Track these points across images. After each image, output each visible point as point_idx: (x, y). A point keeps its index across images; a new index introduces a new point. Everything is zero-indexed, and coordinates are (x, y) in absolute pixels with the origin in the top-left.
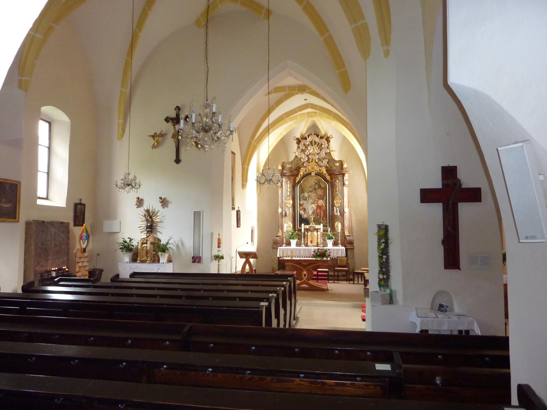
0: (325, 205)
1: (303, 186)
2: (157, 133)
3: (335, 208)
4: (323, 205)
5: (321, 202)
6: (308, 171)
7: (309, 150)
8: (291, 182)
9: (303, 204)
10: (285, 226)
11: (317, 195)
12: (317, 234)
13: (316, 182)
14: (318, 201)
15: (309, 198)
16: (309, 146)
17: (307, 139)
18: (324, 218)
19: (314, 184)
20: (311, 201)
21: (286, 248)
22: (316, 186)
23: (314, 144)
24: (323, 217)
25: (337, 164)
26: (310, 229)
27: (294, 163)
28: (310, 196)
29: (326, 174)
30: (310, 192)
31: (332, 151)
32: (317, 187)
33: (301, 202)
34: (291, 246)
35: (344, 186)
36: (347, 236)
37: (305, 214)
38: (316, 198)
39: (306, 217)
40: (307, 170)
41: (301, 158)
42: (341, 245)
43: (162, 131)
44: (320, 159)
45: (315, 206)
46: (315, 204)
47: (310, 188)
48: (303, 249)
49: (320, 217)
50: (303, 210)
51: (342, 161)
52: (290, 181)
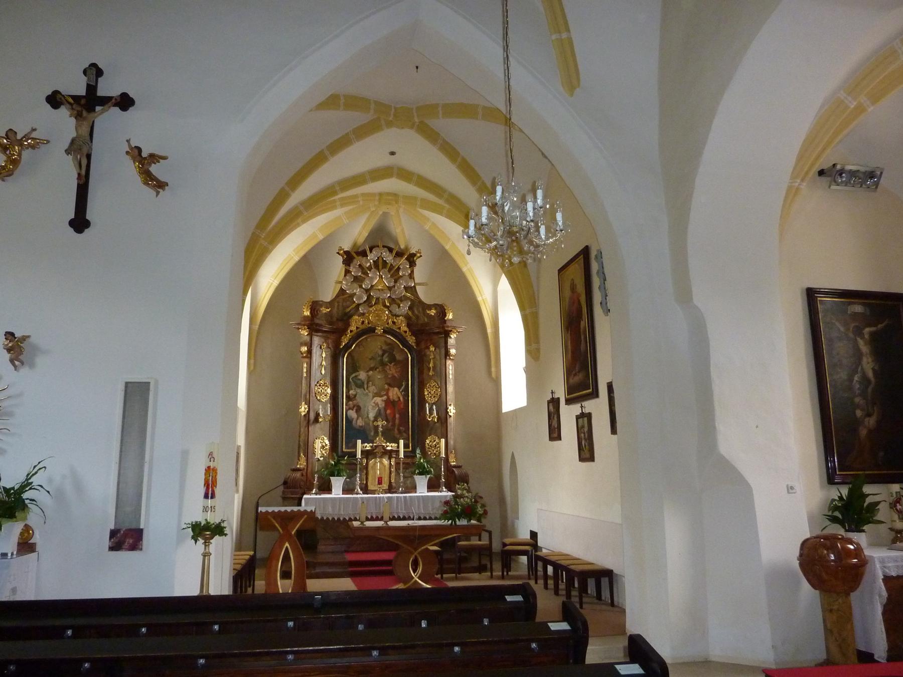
0: (404, 398)
2: (16, 133)
3: (427, 405)
4: (400, 400)
5: (395, 393)
6: (368, 323)
7: (372, 279)
8: (330, 346)
9: (355, 396)
10: (318, 444)
11: (386, 377)
12: (390, 464)
15: (368, 383)
17: (367, 256)
18: (401, 428)
19: (380, 353)
20: (372, 389)
21: (318, 496)
24: (400, 425)
25: (433, 312)
26: (375, 451)
29: (408, 331)
30: (372, 369)
31: (420, 284)
32: (386, 360)
33: (351, 392)
35: (448, 358)
36: (455, 467)
37: (360, 418)
39: (361, 425)
43: (34, 130)
45: (382, 400)
47: (372, 361)
49: (394, 425)
50: (355, 410)
51: (443, 307)
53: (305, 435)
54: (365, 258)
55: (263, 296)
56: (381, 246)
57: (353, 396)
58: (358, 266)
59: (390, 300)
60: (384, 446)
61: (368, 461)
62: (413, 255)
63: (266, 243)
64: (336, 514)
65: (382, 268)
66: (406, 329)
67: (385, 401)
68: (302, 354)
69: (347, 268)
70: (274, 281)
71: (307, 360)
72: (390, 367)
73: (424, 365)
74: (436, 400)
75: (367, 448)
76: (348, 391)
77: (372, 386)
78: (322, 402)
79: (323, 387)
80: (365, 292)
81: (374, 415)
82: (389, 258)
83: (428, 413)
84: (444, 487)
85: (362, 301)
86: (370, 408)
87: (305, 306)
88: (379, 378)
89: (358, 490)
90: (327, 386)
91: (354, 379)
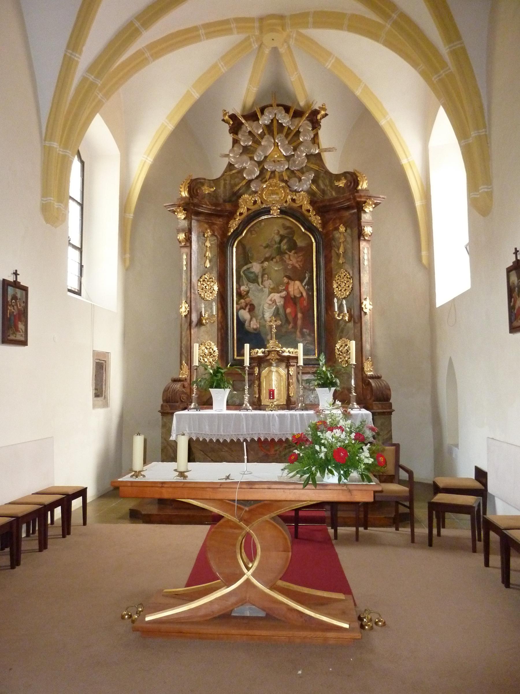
0: (308, 294)
1: (248, 247)
3: (335, 300)
5: (296, 287)
6: (262, 203)
7: (265, 148)
8: (216, 234)
9: (248, 292)
11: (285, 269)
12: (288, 373)
13: (282, 232)
14: (288, 283)
15: (262, 276)
16: (262, 138)
17: (258, 119)
18: (305, 330)
19: (277, 239)
20: (269, 283)
22: (282, 244)
23: (278, 134)
25: (341, 184)
26: (268, 358)
27: (222, 182)
28: (267, 271)
30: (267, 259)
31: (326, 150)
32: (285, 247)
33: (243, 288)
34: (212, 408)
35: (362, 238)
36: (372, 377)
37: (254, 319)
38: (283, 275)
39: (255, 327)
41: (241, 171)
42: (358, 404)
44: (293, 172)
45: (281, 297)
46: (281, 292)
47: (267, 249)
48: (305, 354)
50: (247, 310)
52: (213, 231)
53: (187, 340)
54: (256, 122)
55: (137, 178)
56: (274, 105)
57: (245, 293)
58: (248, 134)
59: (288, 173)
60: (278, 351)
61: (261, 370)
62: (315, 113)
63: (93, 77)
64: (215, 435)
65: (278, 134)
66: (309, 207)
68: (180, 242)
69: (236, 137)
70: (147, 159)
71: (186, 250)
72: (289, 256)
73: (333, 251)
74: (348, 294)
75: (259, 354)
76: (238, 289)
77: (268, 280)
78: (207, 300)
79: (209, 283)
80: (257, 165)
82: (285, 120)
83: (336, 309)
84: (355, 403)
85: (254, 177)
86: (266, 306)
87: (182, 185)
88: (276, 270)
89: (246, 405)
90: (212, 281)
91: (246, 272)
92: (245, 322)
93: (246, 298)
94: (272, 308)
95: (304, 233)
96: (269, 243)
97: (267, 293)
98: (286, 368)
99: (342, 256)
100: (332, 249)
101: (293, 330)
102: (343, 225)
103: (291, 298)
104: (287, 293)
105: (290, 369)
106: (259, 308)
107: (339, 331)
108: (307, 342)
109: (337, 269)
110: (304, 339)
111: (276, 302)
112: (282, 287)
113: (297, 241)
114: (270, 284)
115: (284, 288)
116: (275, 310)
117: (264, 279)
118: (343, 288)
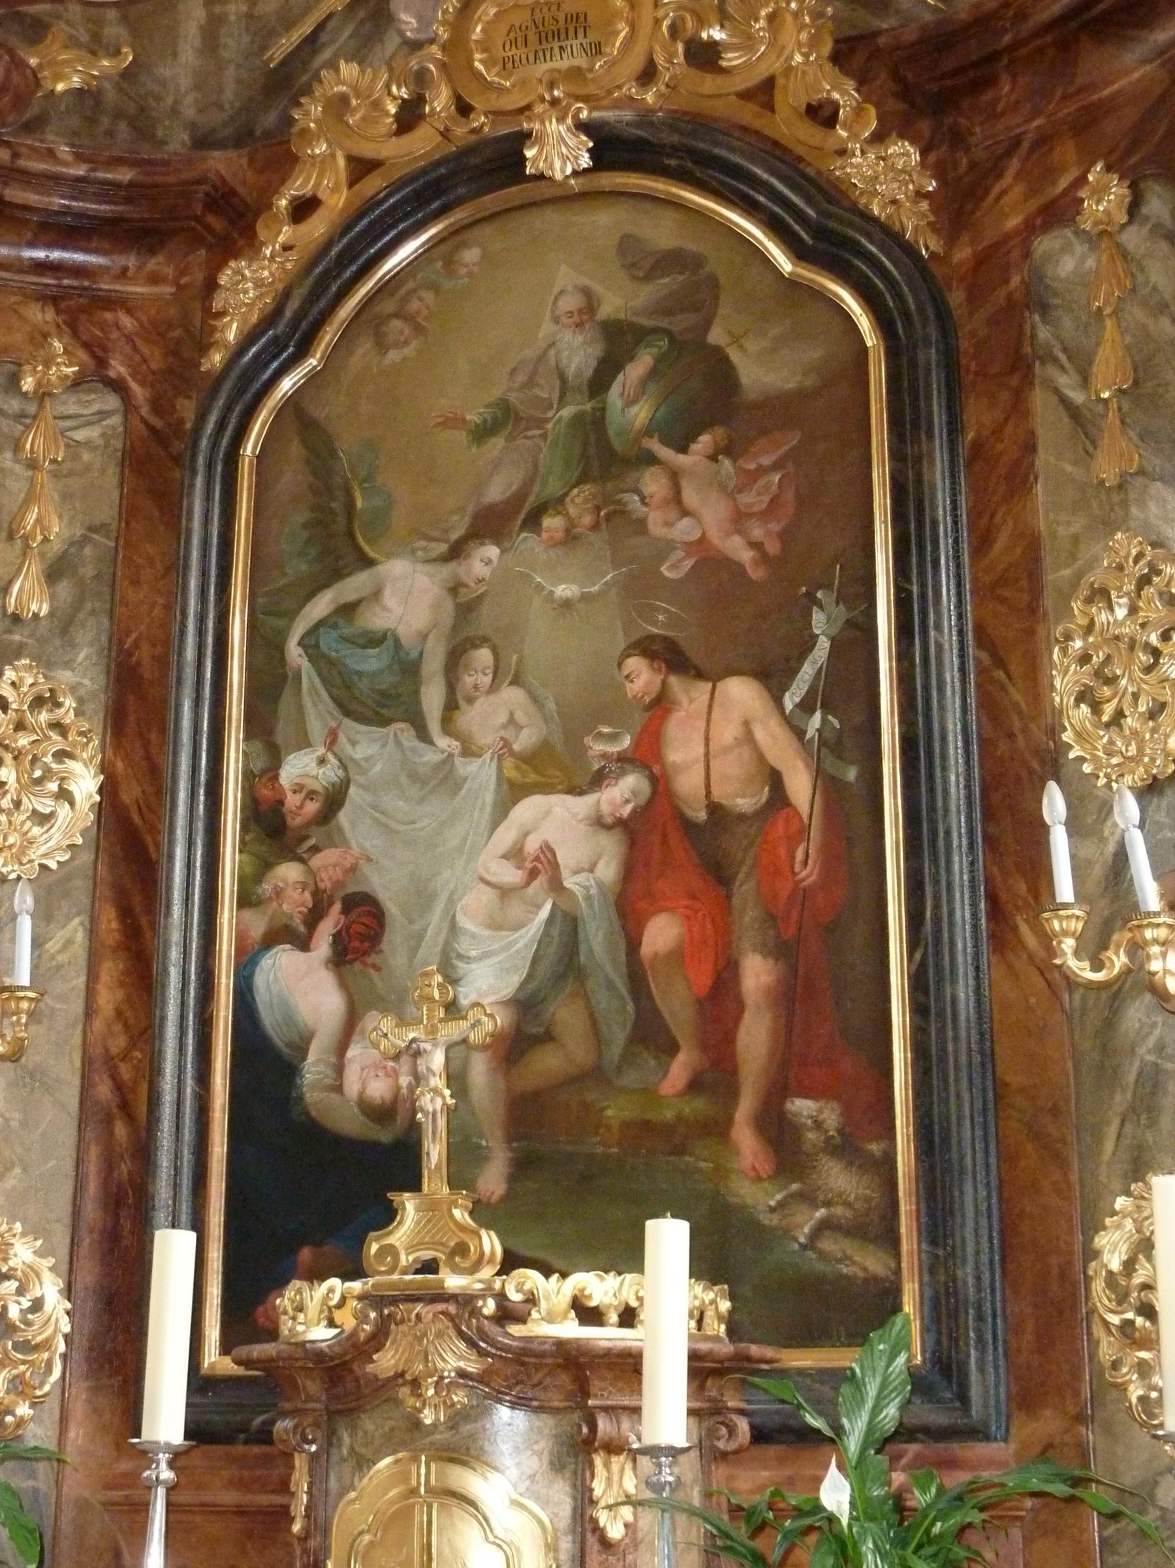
1: (347, 444)
5: (727, 732)
6: (464, 109)
8: (118, 368)
9: (334, 800)
13: (612, 305)
14: (661, 704)
18: (802, 1107)
22: (614, 394)
28: (486, 620)
32: (641, 414)
40: (440, 101)
45: (599, 823)
46: (598, 780)
47: (497, 444)
50: (323, 945)
57: (312, 807)
67: (621, 824)
72: (675, 477)
73: (1040, 401)
77: (494, 688)
81: (510, 984)
88: (567, 604)
91: (328, 642)
92: (303, 1051)
93: (315, 849)
94: (517, 927)
95: (792, 283)
96: (513, 398)
97: (489, 798)
98: (557, 1466)
99: (1112, 416)
100: (1028, 380)
101: (697, 1106)
102: (1109, 168)
103: (688, 826)
104: (654, 780)
105: (598, 1486)
106: (416, 927)
107: (1121, 1100)
108: (821, 1213)
109: (1076, 539)
110: (795, 1187)
111: (555, 865)
112: (613, 738)
113: (734, 355)
114: (512, 721)
115: (626, 742)
116: (546, 933)
117: (468, 680)
118: (1136, 696)
